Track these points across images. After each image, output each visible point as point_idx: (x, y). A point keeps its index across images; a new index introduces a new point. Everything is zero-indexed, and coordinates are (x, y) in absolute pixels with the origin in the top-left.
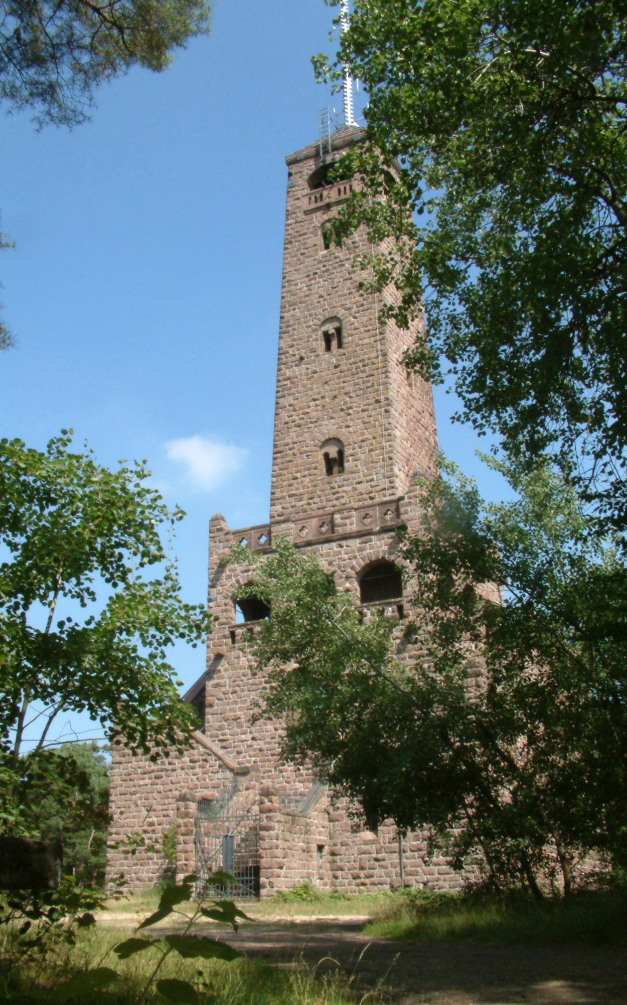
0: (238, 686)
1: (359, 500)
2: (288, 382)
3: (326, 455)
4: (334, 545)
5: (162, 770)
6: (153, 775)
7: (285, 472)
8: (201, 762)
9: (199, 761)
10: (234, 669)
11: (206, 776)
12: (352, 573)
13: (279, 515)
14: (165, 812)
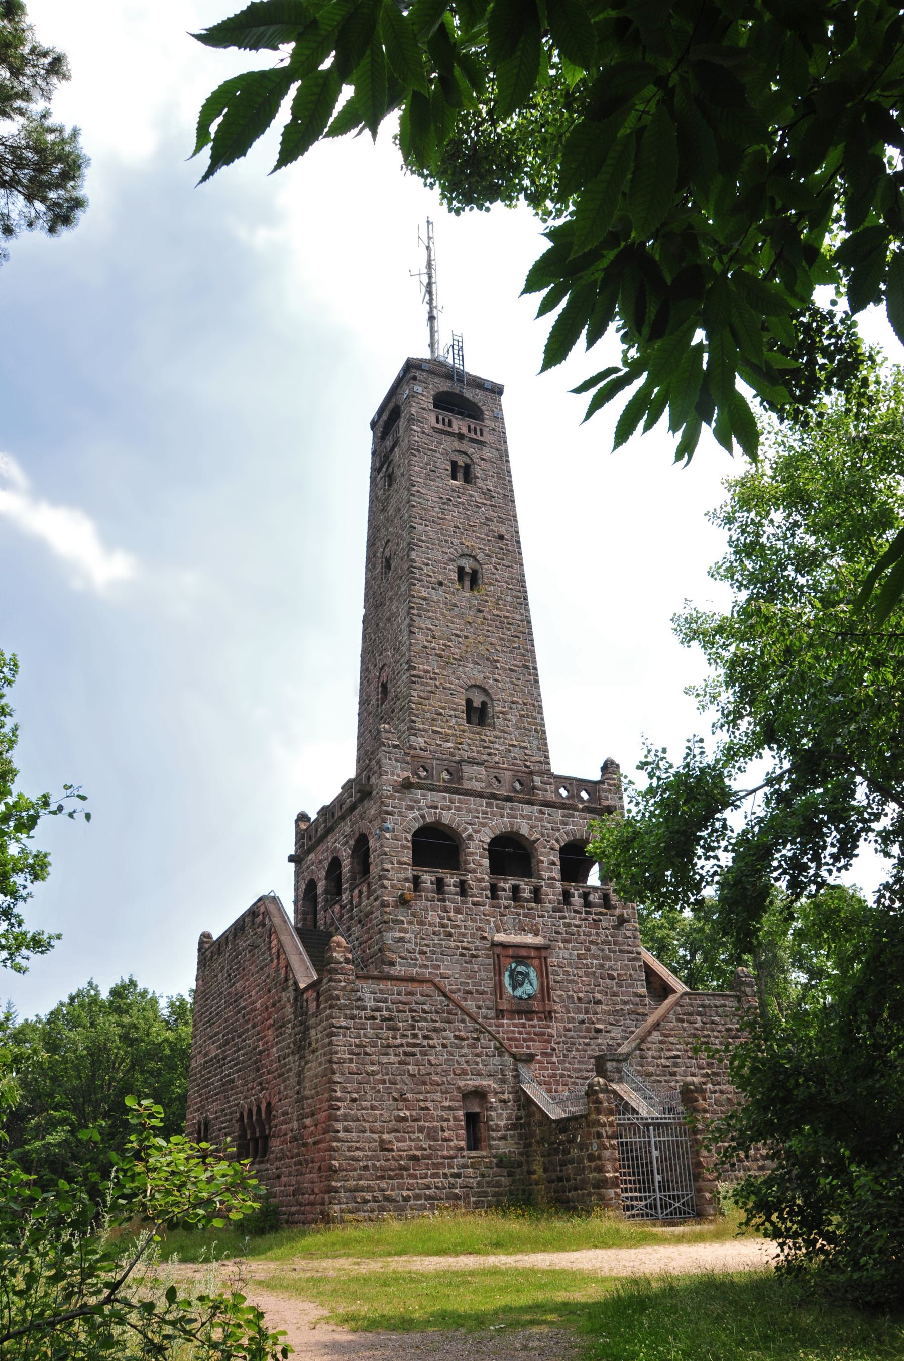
0: (427, 945)
1: (514, 765)
2: (424, 603)
3: (469, 702)
4: (484, 801)
5: (415, 1045)
6: (401, 1050)
7: (427, 702)
8: (470, 1041)
9: (467, 1038)
10: (422, 923)
11: (479, 1059)
12: (557, 846)
13: (421, 749)
14: (422, 1104)
